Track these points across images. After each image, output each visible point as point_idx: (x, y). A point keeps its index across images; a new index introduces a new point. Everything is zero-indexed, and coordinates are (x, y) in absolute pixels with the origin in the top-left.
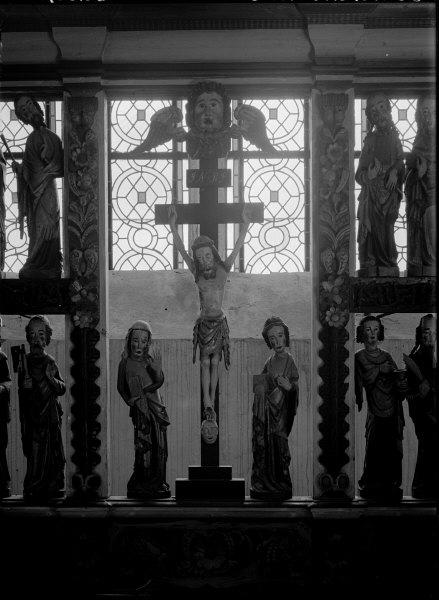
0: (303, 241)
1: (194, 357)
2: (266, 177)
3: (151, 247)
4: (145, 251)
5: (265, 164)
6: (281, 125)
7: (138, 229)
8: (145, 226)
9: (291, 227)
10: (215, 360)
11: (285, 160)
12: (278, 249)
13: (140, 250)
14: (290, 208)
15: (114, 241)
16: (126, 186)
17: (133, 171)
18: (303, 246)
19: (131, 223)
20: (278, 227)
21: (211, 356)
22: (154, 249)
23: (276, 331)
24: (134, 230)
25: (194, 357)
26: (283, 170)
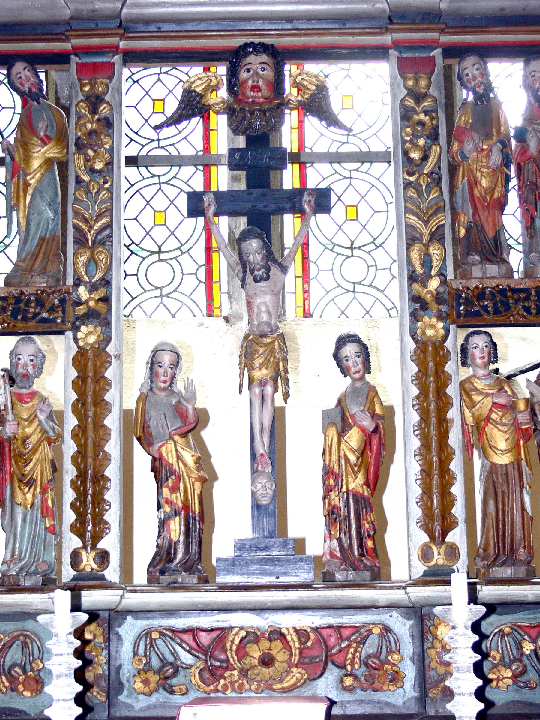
0: (203, 279)
1: (241, 385)
2: (148, 193)
3: (367, 282)
4: (358, 288)
5: (146, 174)
6: (171, 91)
7: (348, 257)
8: (356, 252)
9: (185, 259)
10: (269, 389)
11: (175, 169)
12: (165, 291)
13: (350, 287)
14: (375, 227)
15: (203, 269)
16: (138, 203)
17: (361, 136)
18: (203, 287)
19: (337, 249)
20: (164, 261)
21: (263, 384)
22: (370, 286)
23: (167, 359)
24: (341, 258)
25: (241, 385)
26: (174, 182)
